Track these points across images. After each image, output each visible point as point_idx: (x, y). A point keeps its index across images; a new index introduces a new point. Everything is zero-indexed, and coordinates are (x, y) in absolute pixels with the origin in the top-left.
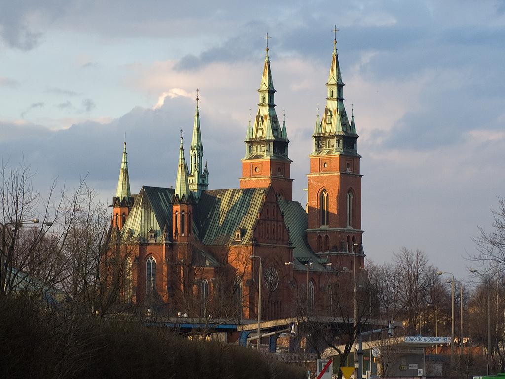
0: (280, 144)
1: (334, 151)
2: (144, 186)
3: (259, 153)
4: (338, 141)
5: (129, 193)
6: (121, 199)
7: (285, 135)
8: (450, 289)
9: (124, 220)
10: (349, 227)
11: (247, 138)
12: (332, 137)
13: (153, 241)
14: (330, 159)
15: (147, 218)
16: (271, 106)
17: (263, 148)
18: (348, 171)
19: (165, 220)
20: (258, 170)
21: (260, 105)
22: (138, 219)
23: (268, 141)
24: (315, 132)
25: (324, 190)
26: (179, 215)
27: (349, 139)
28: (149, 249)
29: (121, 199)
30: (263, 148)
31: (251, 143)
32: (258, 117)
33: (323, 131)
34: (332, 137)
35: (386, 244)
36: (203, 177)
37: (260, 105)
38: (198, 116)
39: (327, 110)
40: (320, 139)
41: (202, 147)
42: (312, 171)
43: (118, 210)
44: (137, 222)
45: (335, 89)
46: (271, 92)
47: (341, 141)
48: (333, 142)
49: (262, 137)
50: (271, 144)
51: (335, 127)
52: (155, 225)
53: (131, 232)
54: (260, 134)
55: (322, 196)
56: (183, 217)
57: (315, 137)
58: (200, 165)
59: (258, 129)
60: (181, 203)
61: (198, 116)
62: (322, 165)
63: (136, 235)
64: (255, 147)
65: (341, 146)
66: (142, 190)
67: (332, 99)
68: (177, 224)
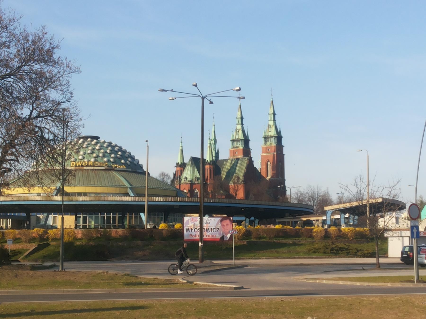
0: (246, 141)
1: (273, 143)
2: (192, 157)
3: (237, 146)
4: (275, 139)
5: (183, 161)
6: (180, 164)
7: (248, 138)
8: (288, 230)
9: (181, 174)
10: (280, 178)
11: (231, 139)
12: (272, 137)
13: (196, 182)
14: (271, 147)
15: (193, 172)
16: (242, 124)
17: (239, 143)
18: (279, 152)
19: (202, 172)
20: (237, 153)
21: (237, 124)
22: (189, 172)
23: (242, 140)
24: (263, 135)
25: (269, 161)
26: (208, 170)
27: (279, 138)
28: (194, 186)
29: (180, 164)
30: (239, 143)
31: (233, 141)
32: (236, 130)
33: (267, 135)
34: (272, 137)
35: (297, 183)
36: (217, 154)
37: (237, 124)
38: (214, 125)
39: (269, 125)
40: (266, 138)
41: (216, 140)
42: (263, 152)
43: (179, 168)
44: (189, 174)
45: (272, 116)
46: (242, 118)
47: (276, 139)
48: (273, 139)
49: (238, 139)
50: (243, 141)
51: (273, 132)
52: (198, 175)
53: (186, 178)
54: (237, 137)
55: (267, 164)
56: (210, 171)
57: (264, 137)
58: (215, 148)
59: (236, 135)
60: (210, 164)
61: (214, 125)
62: (266, 150)
63: (188, 179)
64: (235, 143)
65: (276, 141)
66: (191, 158)
67: (271, 120)
68: (207, 174)
